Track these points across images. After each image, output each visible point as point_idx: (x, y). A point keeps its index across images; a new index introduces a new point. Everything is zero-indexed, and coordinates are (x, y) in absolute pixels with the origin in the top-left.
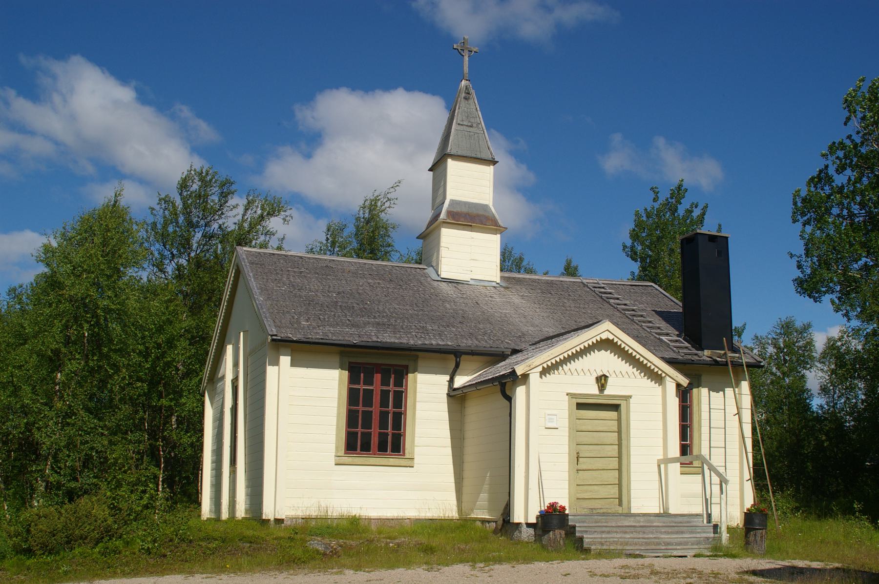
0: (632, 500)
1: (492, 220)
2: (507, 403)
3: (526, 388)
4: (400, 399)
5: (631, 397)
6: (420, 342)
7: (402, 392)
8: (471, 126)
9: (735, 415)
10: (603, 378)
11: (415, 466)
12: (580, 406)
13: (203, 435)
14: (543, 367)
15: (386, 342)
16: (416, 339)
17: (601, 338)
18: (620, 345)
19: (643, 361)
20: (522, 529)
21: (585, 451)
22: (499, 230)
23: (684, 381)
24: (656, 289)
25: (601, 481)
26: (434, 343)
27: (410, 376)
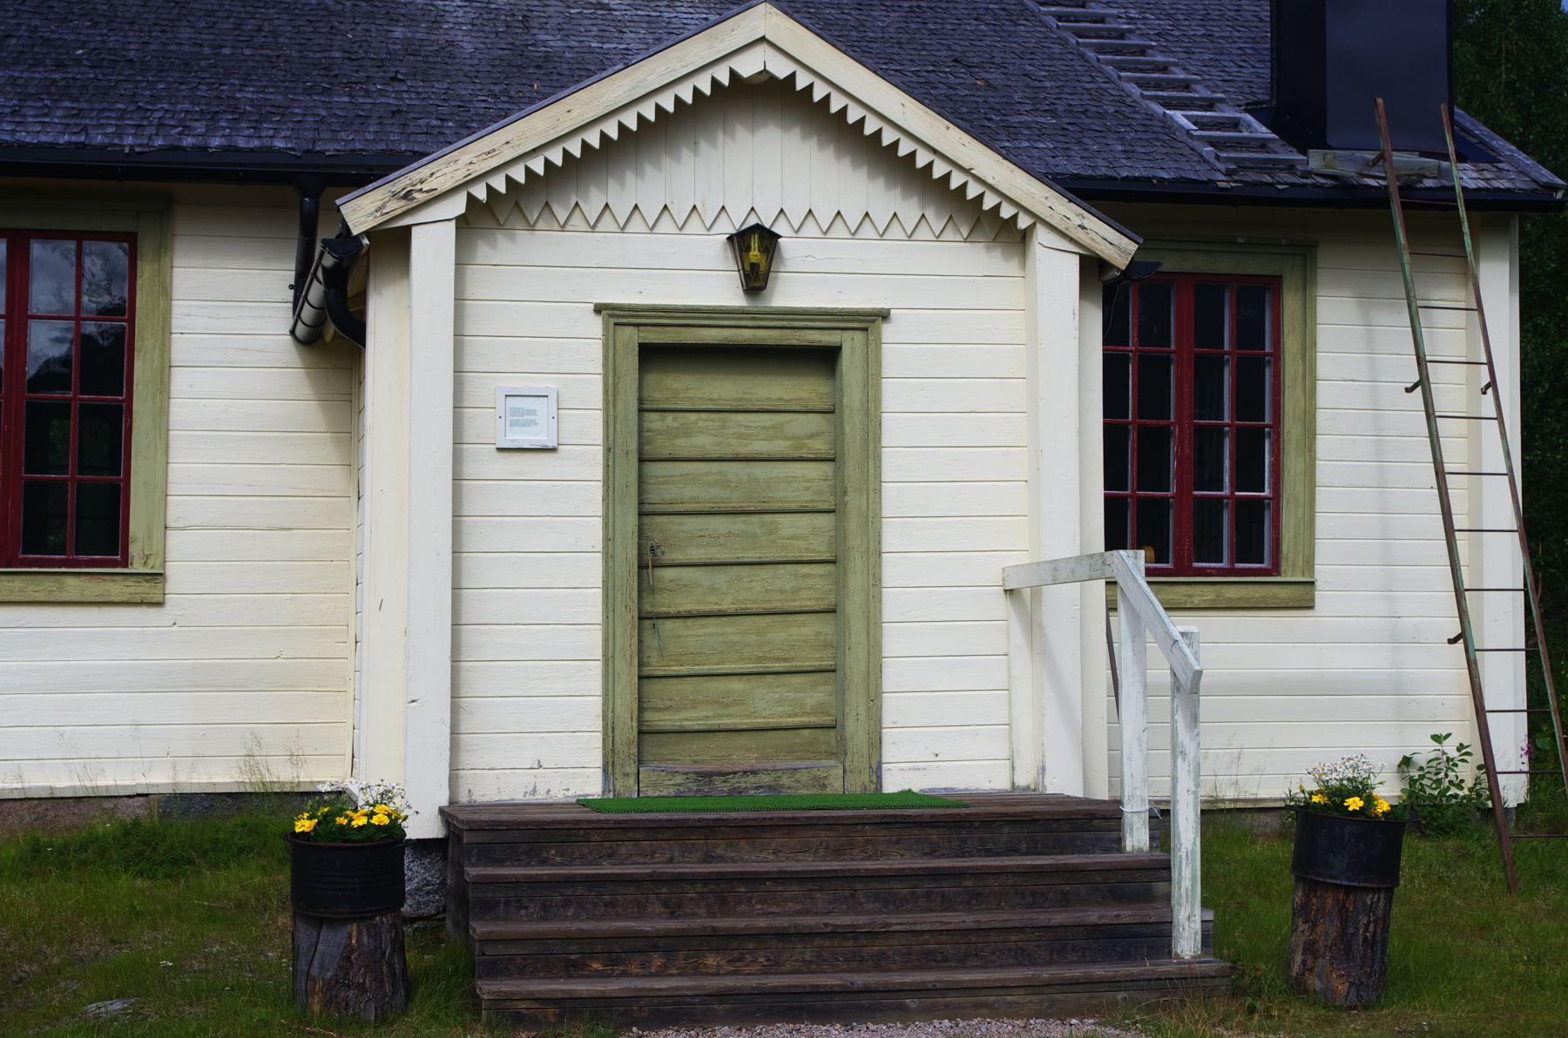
5: (884, 316)
9: (1408, 390)
10: (755, 243)
14: (471, 199)
17: (733, 74)
25: (760, 659)
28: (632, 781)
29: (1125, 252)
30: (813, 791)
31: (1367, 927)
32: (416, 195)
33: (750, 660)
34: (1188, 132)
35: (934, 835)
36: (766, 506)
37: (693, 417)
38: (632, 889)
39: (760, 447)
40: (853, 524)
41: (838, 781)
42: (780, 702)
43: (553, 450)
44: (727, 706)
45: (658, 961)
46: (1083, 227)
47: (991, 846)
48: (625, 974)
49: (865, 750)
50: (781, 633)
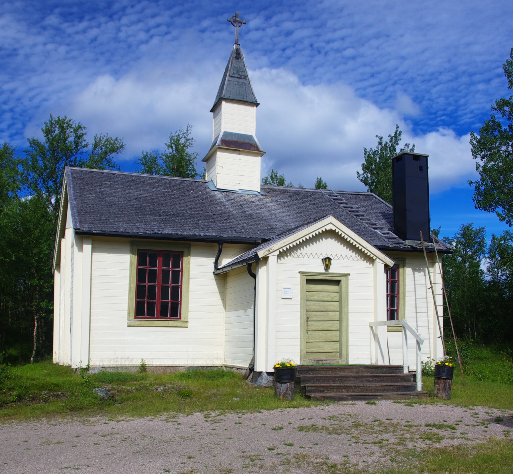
0: (349, 353)
1: (255, 146)
2: (253, 279)
3: (267, 267)
4: (177, 277)
6: (191, 234)
7: (179, 271)
8: (240, 78)
10: (327, 260)
11: (189, 326)
12: (309, 281)
13: (53, 302)
14: (280, 252)
15: (166, 234)
16: (188, 231)
17: (325, 229)
18: (341, 234)
19: (358, 247)
20: (263, 376)
21: (314, 316)
22: (260, 154)
23: (391, 263)
24: (375, 198)
26: (202, 234)
27: (185, 259)
28: (305, 362)
29: (392, 264)
30: (337, 364)
31: (448, 385)
32: (271, 251)
33: (324, 339)
34: (381, 235)
35: (373, 370)
36: (327, 310)
37: (314, 293)
38: (327, 379)
39: (326, 299)
40: (343, 314)
41: (342, 362)
42: (329, 347)
43: (291, 299)
44: (320, 348)
45: (335, 390)
46: (385, 259)
47: (382, 372)
48: (330, 393)
49: (346, 356)
50: (330, 334)
